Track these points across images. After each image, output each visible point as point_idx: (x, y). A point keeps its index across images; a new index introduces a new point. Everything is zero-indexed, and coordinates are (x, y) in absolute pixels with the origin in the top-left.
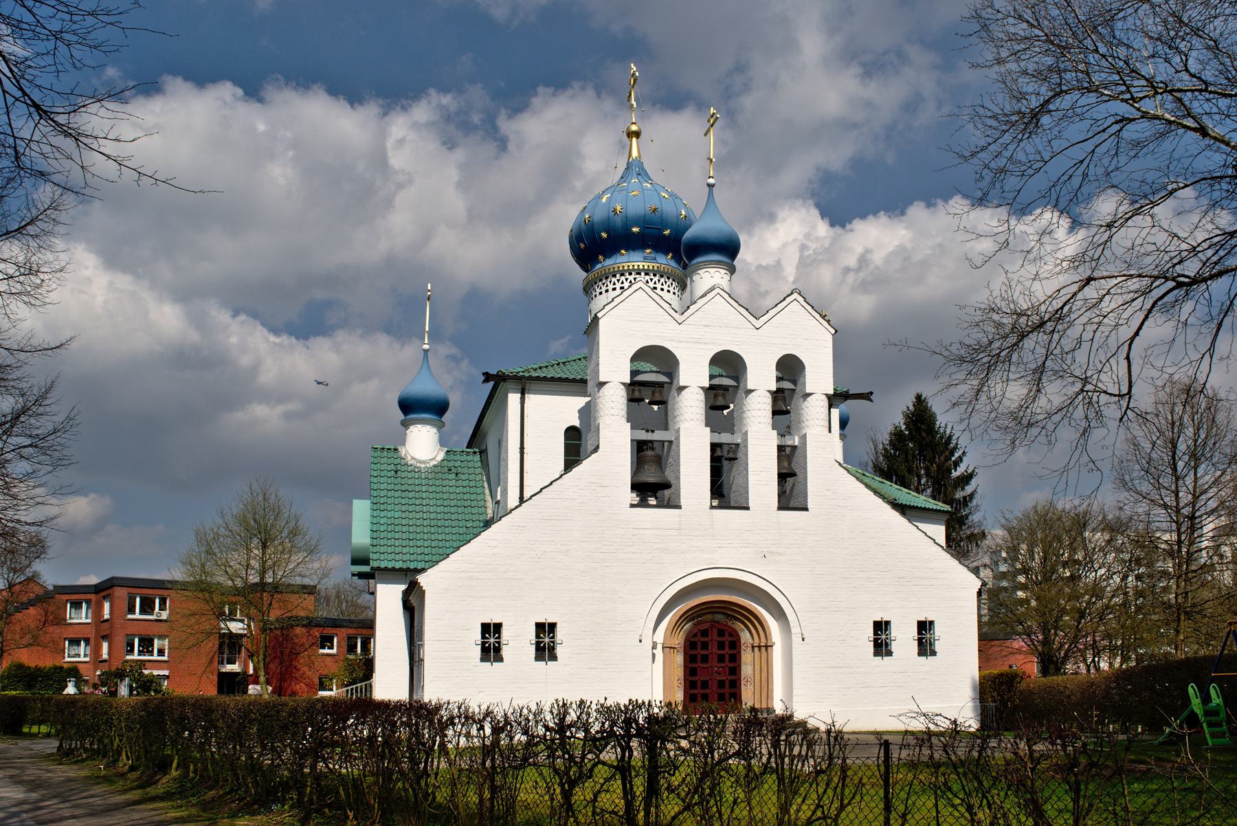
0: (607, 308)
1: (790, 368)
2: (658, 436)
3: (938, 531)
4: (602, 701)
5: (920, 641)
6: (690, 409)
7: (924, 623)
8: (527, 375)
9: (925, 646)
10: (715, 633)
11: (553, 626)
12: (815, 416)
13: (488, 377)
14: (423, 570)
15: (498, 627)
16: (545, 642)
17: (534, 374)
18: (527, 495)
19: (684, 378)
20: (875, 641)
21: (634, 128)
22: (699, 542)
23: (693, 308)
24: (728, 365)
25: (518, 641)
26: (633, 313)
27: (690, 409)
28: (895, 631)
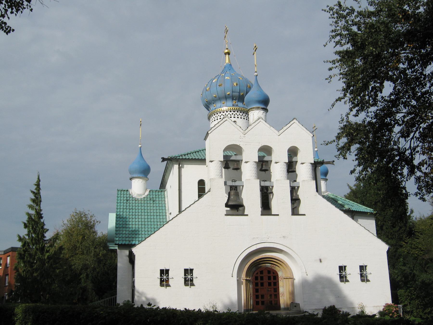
0: (217, 126)
1: (293, 152)
2: (237, 184)
3: (371, 224)
4: (214, 304)
5: (361, 275)
6: (248, 170)
7: (363, 266)
8: (181, 157)
9: (364, 278)
10: (261, 273)
11: (192, 270)
12: (304, 172)
13: (164, 159)
14: (134, 245)
15: (167, 271)
16: (189, 277)
17: (184, 157)
18: (183, 209)
19: (245, 157)
20: (340, 275)
21: (226, 51)
22: (252, 232)
23: (250, 128)
24: (266, 150)
25: (177, 277)
26: (225, 131)
27: (248, 170)
28: (348, 270)
